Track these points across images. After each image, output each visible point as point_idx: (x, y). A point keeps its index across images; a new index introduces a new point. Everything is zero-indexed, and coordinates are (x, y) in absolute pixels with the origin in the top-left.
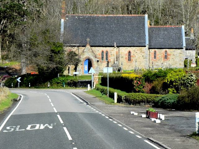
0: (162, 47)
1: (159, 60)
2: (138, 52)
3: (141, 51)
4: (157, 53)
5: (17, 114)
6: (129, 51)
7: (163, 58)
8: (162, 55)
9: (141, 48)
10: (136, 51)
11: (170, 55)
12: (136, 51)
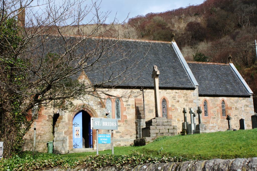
0: (218, 93)
1: (215, 118)
2: (180, 100)
3: (185, 98)
4: (210, 105)
5: (253, 104)
6: (163, 98)
7: (220, 115)
8: (218, 108)
9: (185, 91)
10: (177, 99)
11: (231, 108)
12: (177, 99)
